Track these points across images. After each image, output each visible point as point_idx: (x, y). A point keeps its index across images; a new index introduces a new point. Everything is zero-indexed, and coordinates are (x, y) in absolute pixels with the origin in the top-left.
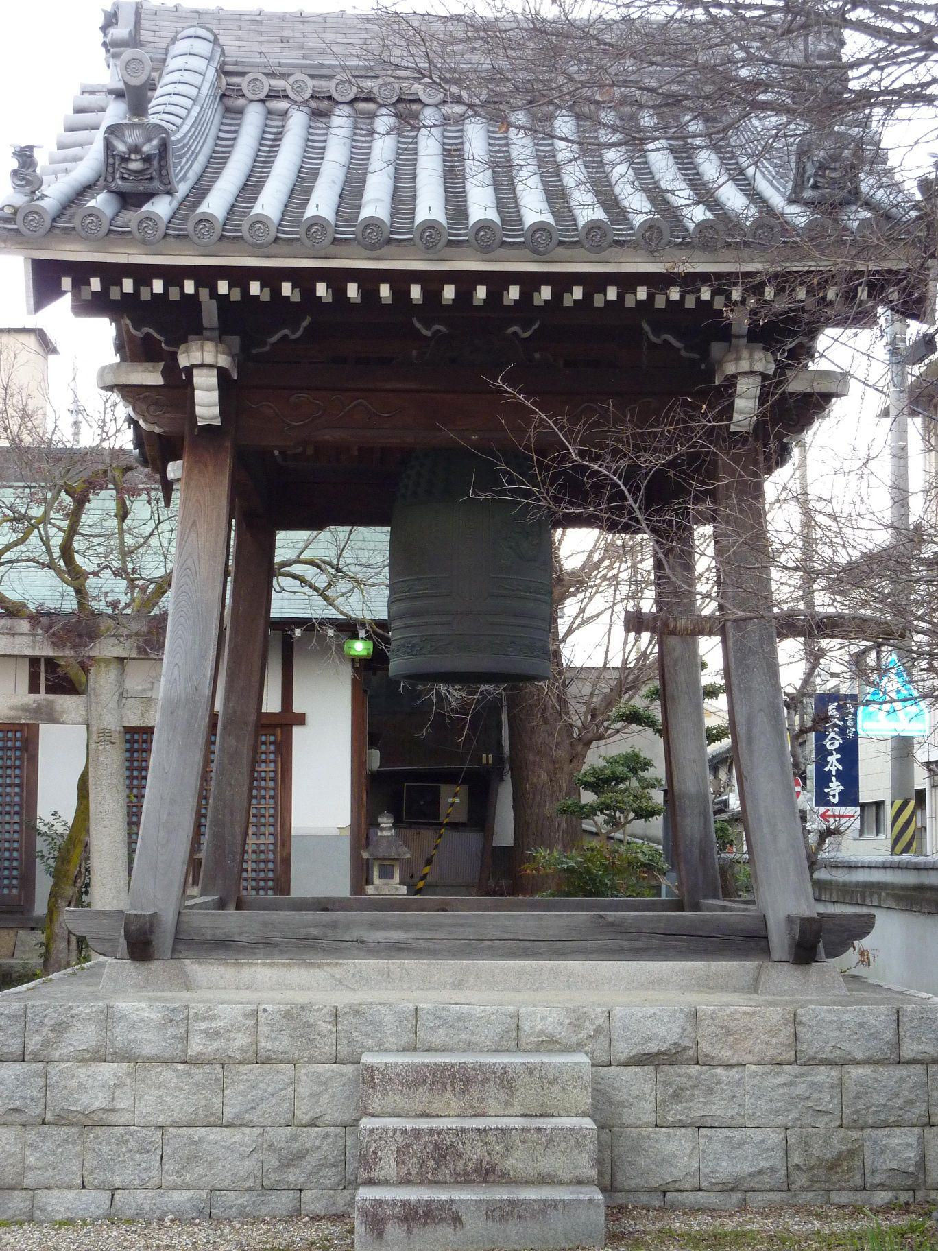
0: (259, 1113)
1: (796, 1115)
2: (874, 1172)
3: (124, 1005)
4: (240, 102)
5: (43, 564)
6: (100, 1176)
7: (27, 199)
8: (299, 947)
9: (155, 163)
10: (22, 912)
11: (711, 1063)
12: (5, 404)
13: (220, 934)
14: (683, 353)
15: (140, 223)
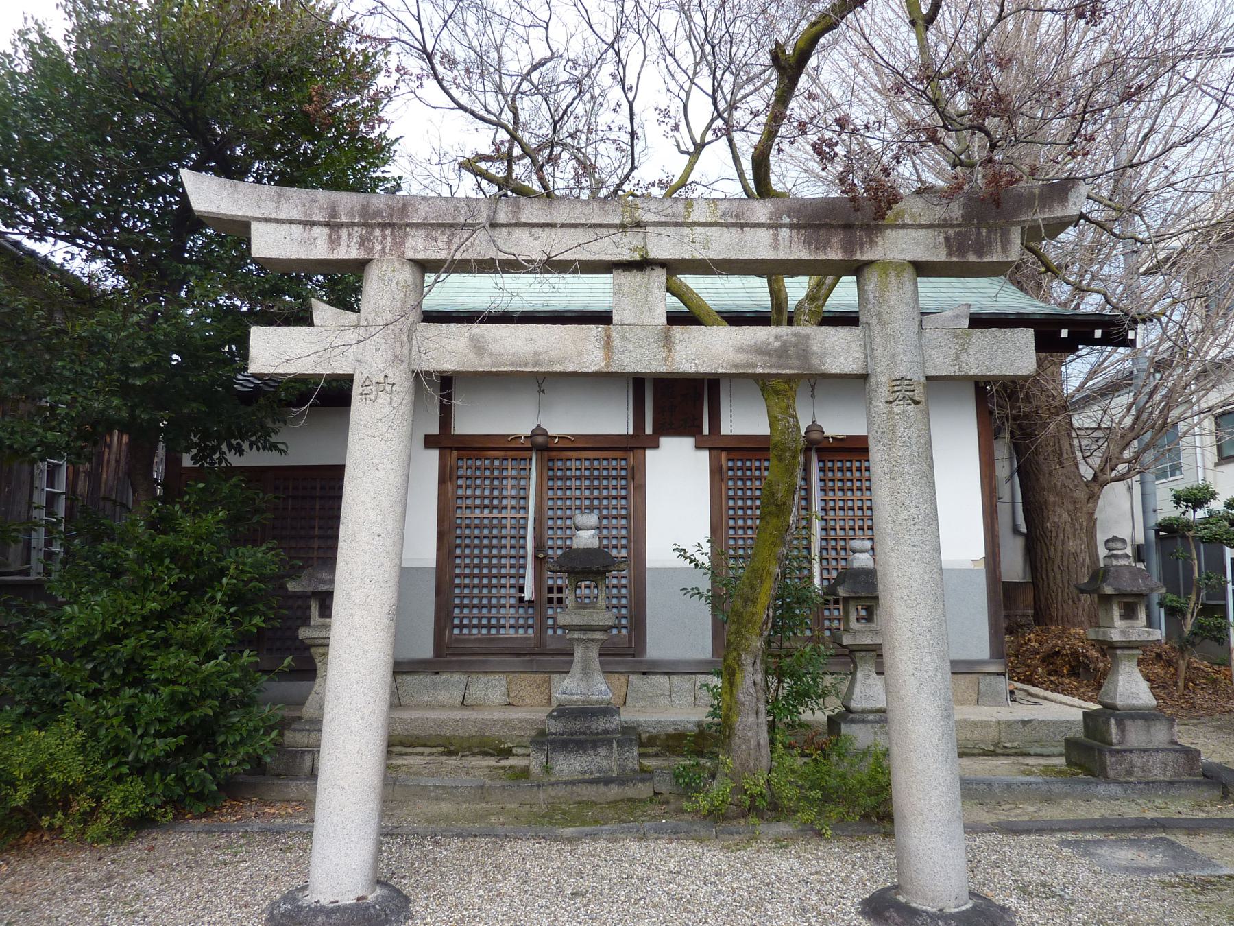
10: (633, 655)
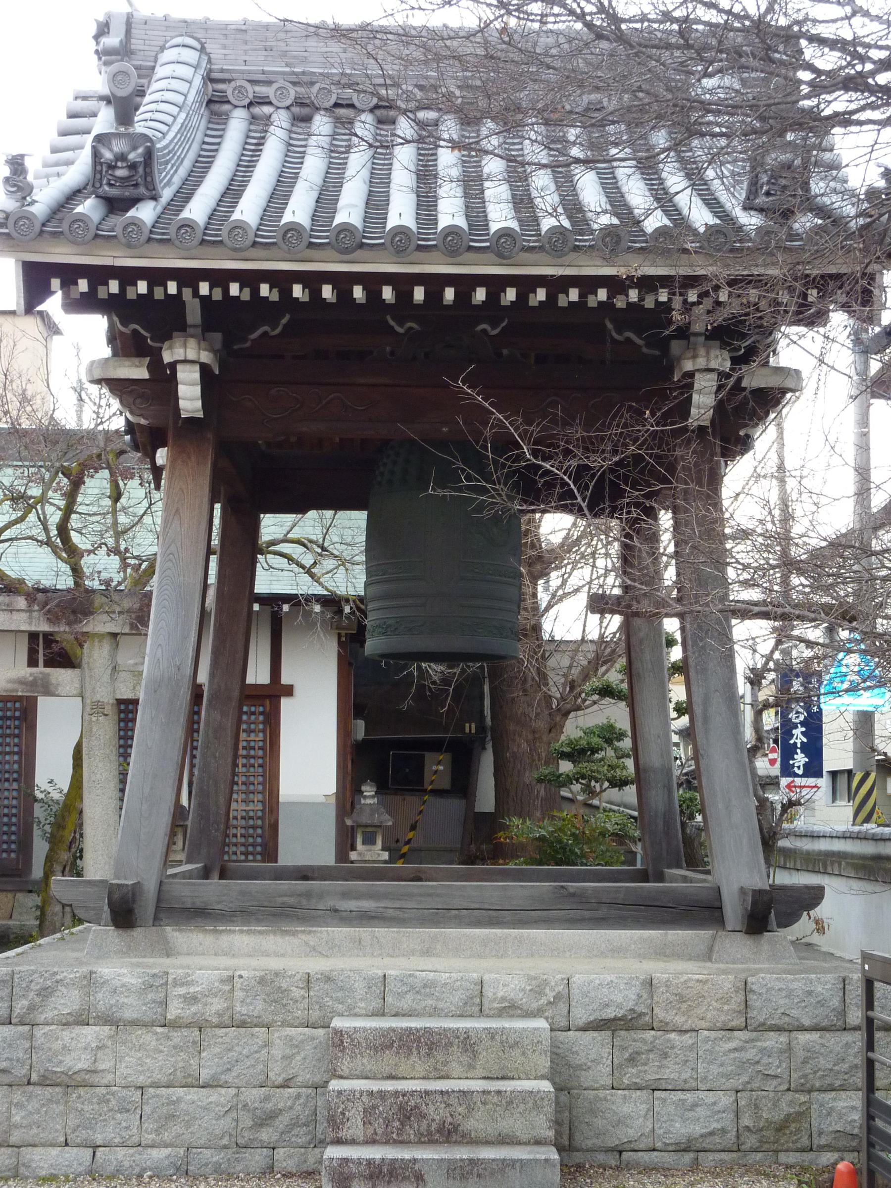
0: (234, 1074)
1: (746, 1079)
2: (820, 1134)
3: (107, 971)
4: (226, 107)
5: (41, 542)
6: (83, 1134)
7: (18, 204)
8: (274, 915)
9: (141, 170)
10: (20, 876)
11: (665, 1028)
12: (5, 389)
13: (199, 904)
14: (645, 350)
15: (125, 228)
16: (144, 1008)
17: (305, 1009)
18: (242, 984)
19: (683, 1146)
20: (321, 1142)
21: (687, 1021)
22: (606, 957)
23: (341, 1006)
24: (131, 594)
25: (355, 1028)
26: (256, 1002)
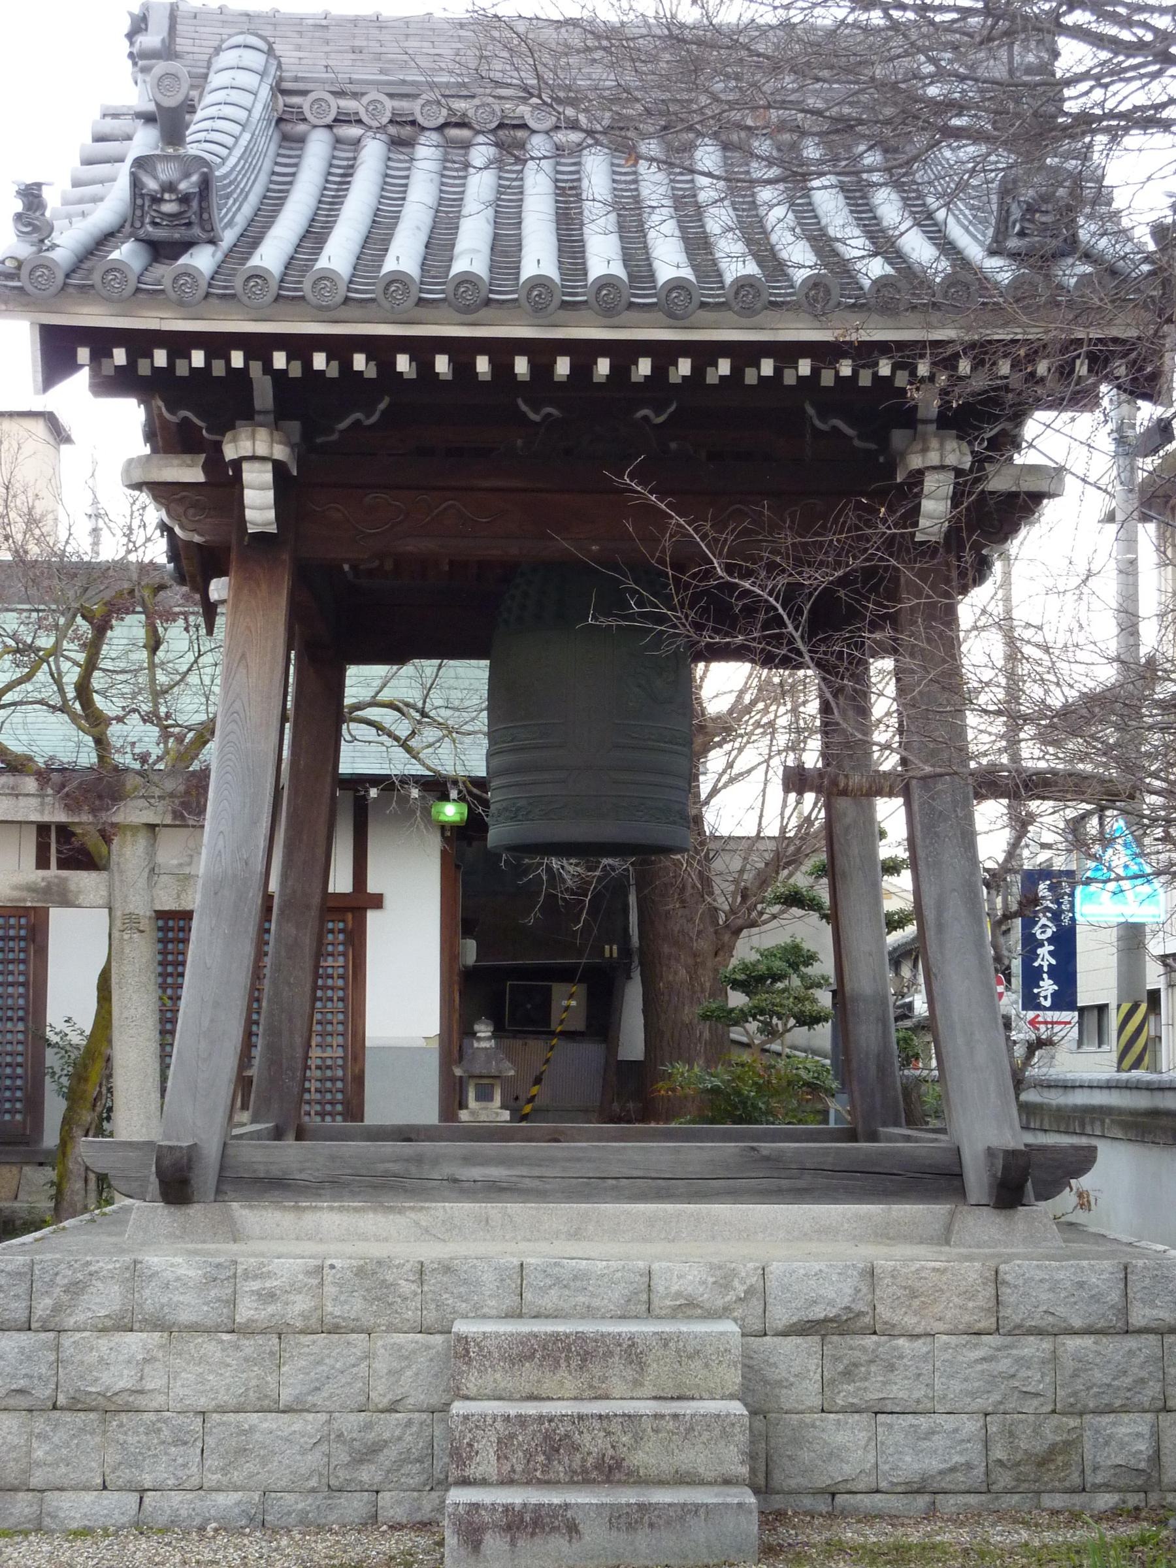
1: (999, 1398)
2: (1096, 1469)
3: (156, 1259)
4: (302, 128)
5: (53, 707)
6: (126, 1474)
7: (34, 249)
8: (375, 1187)
9: (195, 204)
10: (27, 1144)
11: (891, 1332)
12: (6, 506)
13: (275, 1171)
14: (857, 443)
15: (175, 280)
16: (206, 1308)
17: (417, 1309)
18: (334, 1276)
19: (915, 1486)
20: (439, 1483)
21: (919, 1323)
22: (811, 1240)
23: (464, 1305)
24: (172, 772)
25: (484, 1333)
26: (353, 1300)
